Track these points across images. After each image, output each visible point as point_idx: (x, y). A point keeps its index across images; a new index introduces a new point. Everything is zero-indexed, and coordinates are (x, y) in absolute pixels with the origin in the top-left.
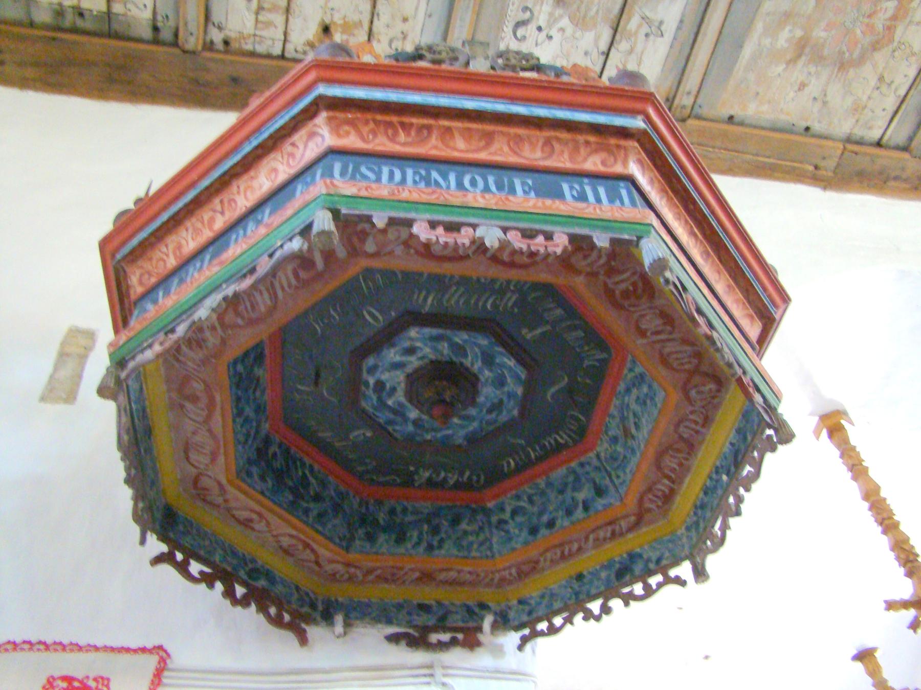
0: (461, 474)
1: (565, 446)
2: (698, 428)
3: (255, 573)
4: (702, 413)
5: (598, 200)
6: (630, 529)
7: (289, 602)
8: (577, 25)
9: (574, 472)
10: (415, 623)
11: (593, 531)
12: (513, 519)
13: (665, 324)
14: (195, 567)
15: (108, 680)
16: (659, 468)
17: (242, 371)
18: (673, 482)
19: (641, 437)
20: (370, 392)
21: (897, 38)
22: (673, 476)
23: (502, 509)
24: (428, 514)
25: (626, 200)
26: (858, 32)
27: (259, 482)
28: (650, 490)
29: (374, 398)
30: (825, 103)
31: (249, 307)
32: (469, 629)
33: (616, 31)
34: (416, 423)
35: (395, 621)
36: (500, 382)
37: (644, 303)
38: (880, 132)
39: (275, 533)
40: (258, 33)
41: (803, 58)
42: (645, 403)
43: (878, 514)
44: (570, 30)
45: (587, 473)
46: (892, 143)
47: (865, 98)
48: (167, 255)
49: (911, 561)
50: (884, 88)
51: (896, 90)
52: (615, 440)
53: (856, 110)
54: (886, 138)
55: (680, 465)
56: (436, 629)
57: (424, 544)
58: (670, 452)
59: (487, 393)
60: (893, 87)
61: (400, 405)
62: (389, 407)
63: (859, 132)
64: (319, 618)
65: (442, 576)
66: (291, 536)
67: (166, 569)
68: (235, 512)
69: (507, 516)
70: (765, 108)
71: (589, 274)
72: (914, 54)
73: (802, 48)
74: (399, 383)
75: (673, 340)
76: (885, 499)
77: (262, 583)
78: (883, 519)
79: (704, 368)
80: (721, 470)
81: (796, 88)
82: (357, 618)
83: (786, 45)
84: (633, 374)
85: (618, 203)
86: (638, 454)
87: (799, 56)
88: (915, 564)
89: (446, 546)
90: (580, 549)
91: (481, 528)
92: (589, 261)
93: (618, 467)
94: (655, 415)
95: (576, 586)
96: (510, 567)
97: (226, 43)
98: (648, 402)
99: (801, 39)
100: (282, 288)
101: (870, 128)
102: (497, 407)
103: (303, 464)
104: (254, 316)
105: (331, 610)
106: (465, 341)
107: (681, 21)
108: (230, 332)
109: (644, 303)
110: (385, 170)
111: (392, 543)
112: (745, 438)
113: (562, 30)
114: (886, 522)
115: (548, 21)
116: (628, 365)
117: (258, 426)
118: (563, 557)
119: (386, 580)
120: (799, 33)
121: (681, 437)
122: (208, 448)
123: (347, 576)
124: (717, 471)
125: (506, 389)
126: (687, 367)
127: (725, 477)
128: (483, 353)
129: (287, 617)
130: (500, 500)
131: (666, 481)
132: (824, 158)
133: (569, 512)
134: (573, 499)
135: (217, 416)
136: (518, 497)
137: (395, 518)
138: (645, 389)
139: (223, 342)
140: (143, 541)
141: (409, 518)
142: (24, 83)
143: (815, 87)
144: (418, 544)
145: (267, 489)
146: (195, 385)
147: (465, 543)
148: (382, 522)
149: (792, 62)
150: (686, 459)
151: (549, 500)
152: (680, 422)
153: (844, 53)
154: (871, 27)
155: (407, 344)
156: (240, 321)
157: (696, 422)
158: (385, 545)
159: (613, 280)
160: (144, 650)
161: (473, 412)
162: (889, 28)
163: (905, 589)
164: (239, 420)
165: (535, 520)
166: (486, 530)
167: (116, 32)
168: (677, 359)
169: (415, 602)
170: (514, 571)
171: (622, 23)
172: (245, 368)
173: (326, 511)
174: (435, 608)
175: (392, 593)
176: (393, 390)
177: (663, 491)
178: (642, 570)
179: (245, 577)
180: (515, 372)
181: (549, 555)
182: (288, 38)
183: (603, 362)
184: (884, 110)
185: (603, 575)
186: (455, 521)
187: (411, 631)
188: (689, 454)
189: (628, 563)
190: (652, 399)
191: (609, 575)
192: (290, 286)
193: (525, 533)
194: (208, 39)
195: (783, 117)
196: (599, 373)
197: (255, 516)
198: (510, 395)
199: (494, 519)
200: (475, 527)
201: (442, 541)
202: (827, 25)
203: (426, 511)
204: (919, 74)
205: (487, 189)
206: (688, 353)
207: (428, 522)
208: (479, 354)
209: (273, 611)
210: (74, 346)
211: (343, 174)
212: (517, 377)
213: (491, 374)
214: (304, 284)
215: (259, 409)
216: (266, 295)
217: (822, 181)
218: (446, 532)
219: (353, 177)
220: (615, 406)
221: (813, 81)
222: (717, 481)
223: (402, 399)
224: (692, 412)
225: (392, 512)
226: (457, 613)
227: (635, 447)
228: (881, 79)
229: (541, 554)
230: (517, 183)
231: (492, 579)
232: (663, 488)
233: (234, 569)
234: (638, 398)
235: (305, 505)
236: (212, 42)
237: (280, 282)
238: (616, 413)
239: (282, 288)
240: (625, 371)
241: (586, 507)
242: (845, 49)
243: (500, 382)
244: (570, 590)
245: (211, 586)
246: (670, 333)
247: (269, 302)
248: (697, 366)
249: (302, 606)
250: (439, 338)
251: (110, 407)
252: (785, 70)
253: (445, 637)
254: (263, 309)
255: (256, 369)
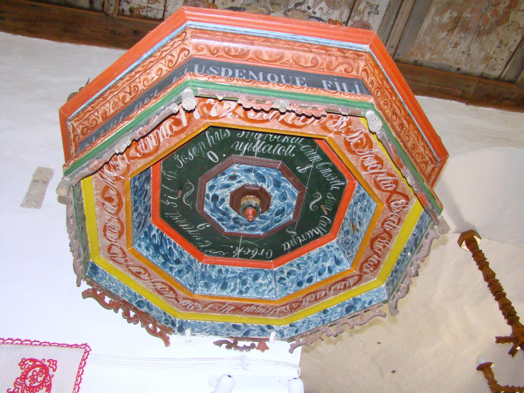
0: (259, 251)
1: (319, 236)
2: (394, 225)
3: (140, 303)
4: (397, 216)
5: (343, 90)
6: (355, 284)
7: (160, 321)
8: (330, 6)
9: (324, 251)
10: (231, 335)
11: (334, 284)
12: (288, 277)
13: (378, 163)
14: (107, 300)
15: (56, 361)
16: (372, 248)
17: (138, 185)
18: (379, 257)
19: (362, 230)
20: (209, 201)
21: (510, 19)
22: (380, 253)
23: (282, 272)
24: (240, 273)
25: (358, 91)
26: (489, 14)
27: (145, 250)
28: (366, 261)
29: (212, 204)
30: (469, 55)
31: (144, 147)
32: (261, 339)
33: (352, 10)
34: (235, 220)
35: (220, 334)
36: (283, 198)
37: (367, 151)
38: (500, 72)
39: (153, 281)
40: (149, 5)
41: (457, 29)
42: (365, 210)
43: (494, 289)
44: (325, 9)
45: (331, 252)
46: (506, 79)
47: (492, 52)
48: (98, 117)
49: (512, 315)
50: (503, 47)
51: (509, 48)
52: (347, 232)
53: (486, 59)
54: (503, 76)
55: (384, 247)
56: (242, 339)
57: (237, 290)
58: (379, 239)
59: (276, 204)
60: (508, 46)
61: (226, 209)
62: (220, 210)
63: (488, 72)
64: (176, 331)
65: (247, 309)
66: (162, 283)
67: (92, 301)
68: (131, 268)
69: (285, 275)
70: (435, 56)
71: (336, 133)
72: (520, 28)
73: (457, 24)
74: (226, 196)
75: (383, 173)
76: (498, 280)
77: (145, 309)
78: (496, 292)
79: (398, 190)
80: (407, 250)
81: (453, 46)
82: (198, 332)
83: (448, 21)
84: (358, 194)
85: (353, 92)
86: (360, 240)
87: (455, 28)
88: (514, 317)
89: (250, 291)
90: (326, 295)
91: (270, 282)
92: (336, 125)
93: (349, 247)
94: (371, 217)
95: (323, 316)
96: (286, 305)
97: (131, 10)
98: (367, 210)
99: (456, 18)
100: (163, 136)
101: (494, 70)
102: (281, 212)
103: (170, 243)
104: (146, 152)
105: (184, 327)
106: (264, 172)
107: (389, 6)
108: (132, 161)
109: (367, 151)
110: (223, 69)
111: (219, 289)
112: (422, 231)
113: (321, 9)
114: (498, 293)
115: (314, 3)
116: (356, 189)
117: (146, 218)
118: (316, 299)
119: (215, 311)
120: (455, 14)
121: (385, 231)
122: (117, 229)
123: (193, 307)
124: (405, 251)
125: (286, 201)
126: (389, 189)
127: (409, 254)
128: (274, 180)
129: (159, 330)
130: (281, 266)
131: (375, 256)
132: (468, 86)
133: (320, 274)
134: (323, 266)
135: (123, 210)
136: (291, 265)
137: (221, 275)
138: (365, 203)
139: (129, 166)
140: (79, 285)
141: (230, 275)
142: (15, 31)
143: (463, 46)
144: (234, 290)
145: (150, 255)
146: (111, 191)
147: (260, 290)
148: (214, 277)
149: (451, 31)
150: (387, 243)
151: (309, 267)
152: (385, 221)
153: (480, 26)
154: (496, 12)
155: (231, 174)
156: (138, 155)
157: (394, 222)
158: (215, 290)
159: (349, 137)
160: (77, 346)
161: (267, 214)
162: (506, 13)
163: (507, 331)
164: (135, 214)
165: (301, 278)
166: (273, 283)
167: (69, 3)
168: (384, 184)
169: (232, 324)
170: (288, 307)
171: (355, 6)
172: (140, 183)
173: (182, 269)
174: (242, 328)
175: (217, 319)
176: (223, 200)
177: (374, 262)
178: (361, 307)
179: (136, 305)
180: (292, 192)
181: (308, 298)
182: (167, 9)
183: (342, 187)
184: (502, 60)
185: (339, 310)
186: (256, 278)
187: (228, 339)
188: (389, 241)
189: (353, 303)
190: (369, 208)
191: (342, 310)
192: (167, 135)
193: (295, 285)
194: (121, 8)
195: (444, 62)
196: (339, 193)
197: (142, 270)
198: (289, 205)
199: (278, 277)
200: (267, 281)
201: (248, 289)
202: (471, 10)
203: (239, 272)
204: (522, 39)
205: (280, 81)
206: (390, 181)
207: (240, 278)
208: (272, 180)
209: (151, 326)
210: (41, 179)
211: (199, 71)
212: (293, 195)
213: (279, 193)
214: (177, 133)
215: (147, 209)
216: (154, 140)
217: (466, 99)
218: (250, 284)
219: (205, 72)
220: (348, 213)
221: (463, 41)
222: (405, 256)
223: (228, 206)
224: (392, 216)
225: (220, 271)
226: (255, 330)
227: (359, 236)
228: (501, 42)
229: (304, 298)
230: (297, 79)
231: (275, 312)
232: (373, 260)
233: (130, 301)
234: (361, 207)
235: (171, 265)
236: (123, 10)
237: (162, 133)
238: (348, 217)
239: (163, 136)
240: (354, 193)
241: (330, 271)
242: (481, 24)
243: (283, 198)
244: (319, 318)
245: (116, 311)
246: (381, 169)
247: (155, 144)
248: (395, 189)
249: (167, 324)
250: (249, 171)
251: (63, 207)
252: (447, 35)
253: (248, 344)
254: (151, 148)
255: (146, 185)
